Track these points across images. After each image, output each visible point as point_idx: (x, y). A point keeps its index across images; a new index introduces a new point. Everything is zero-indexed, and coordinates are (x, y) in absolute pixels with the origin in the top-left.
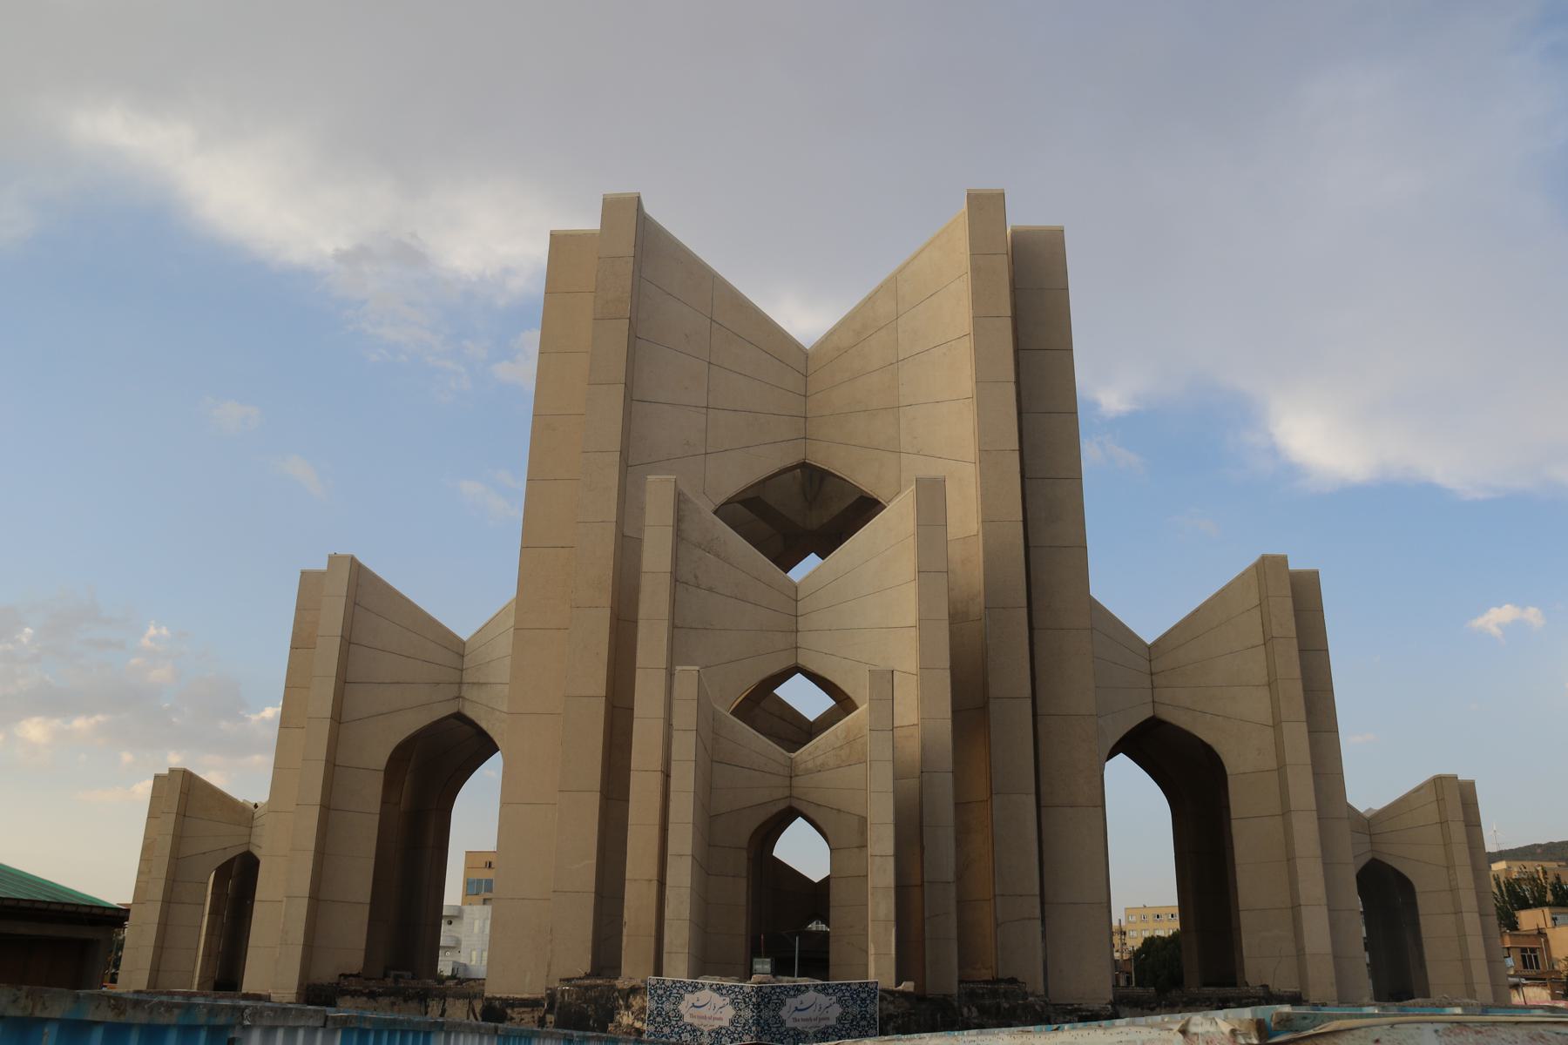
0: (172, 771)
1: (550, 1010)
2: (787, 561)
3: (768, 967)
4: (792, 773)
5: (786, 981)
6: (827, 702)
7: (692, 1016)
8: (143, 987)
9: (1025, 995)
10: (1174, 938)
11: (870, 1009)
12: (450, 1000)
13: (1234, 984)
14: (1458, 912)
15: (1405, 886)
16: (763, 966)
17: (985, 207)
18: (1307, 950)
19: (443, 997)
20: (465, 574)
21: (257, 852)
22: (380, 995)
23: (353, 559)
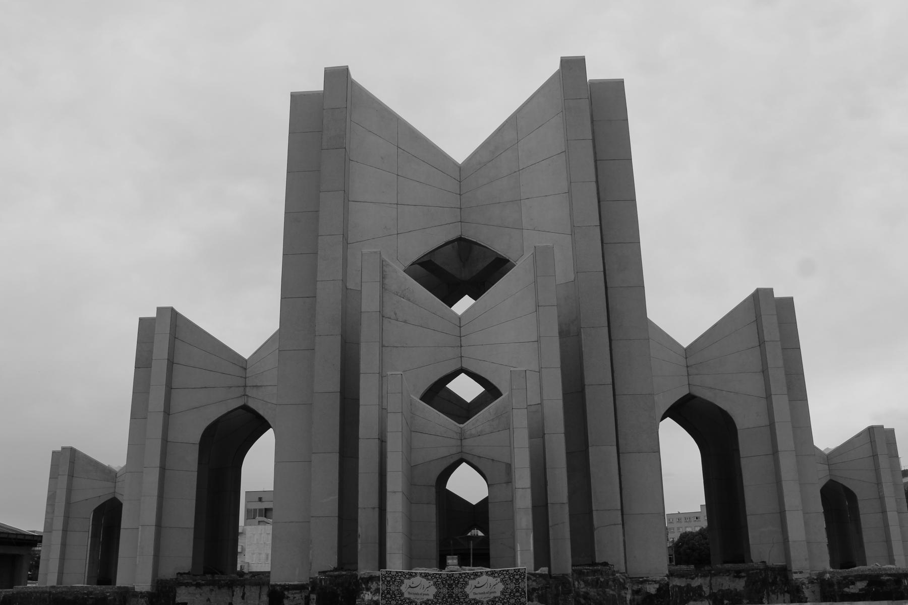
0: (63, 448)
1: (312, 592)
2: (451, 301)
3: (456, 561)
4: (462, 437)
5: (467, 570)
6: (480, 389)
7: (409, 593)
8: (55, 584)
9: (614, 573)
10: (701, 532)
11: (522, 585)
12: (247, 587)
13: (743, 562)
14: (884, 512)
15: (851, 496)
16: (452, 561)
17: (573, 67)
18: (790, 539)
19: (243, 585)
20: (245, 317)
21: (120, 498)
22: (204, 585)
23: (172, 309)
